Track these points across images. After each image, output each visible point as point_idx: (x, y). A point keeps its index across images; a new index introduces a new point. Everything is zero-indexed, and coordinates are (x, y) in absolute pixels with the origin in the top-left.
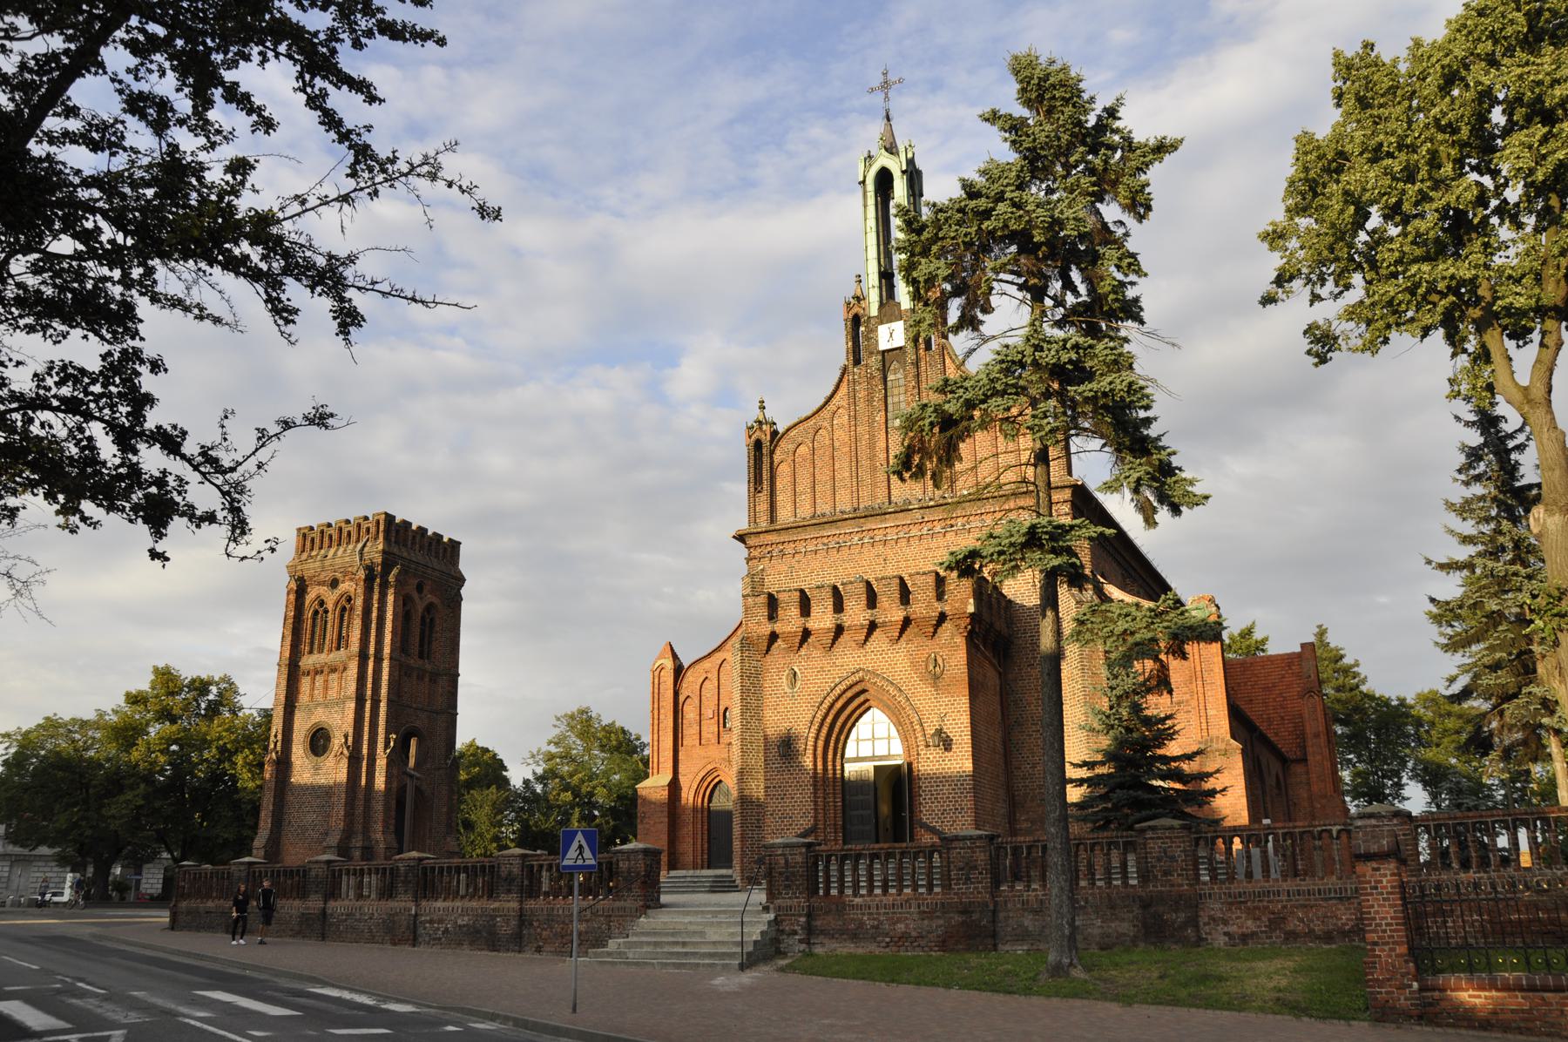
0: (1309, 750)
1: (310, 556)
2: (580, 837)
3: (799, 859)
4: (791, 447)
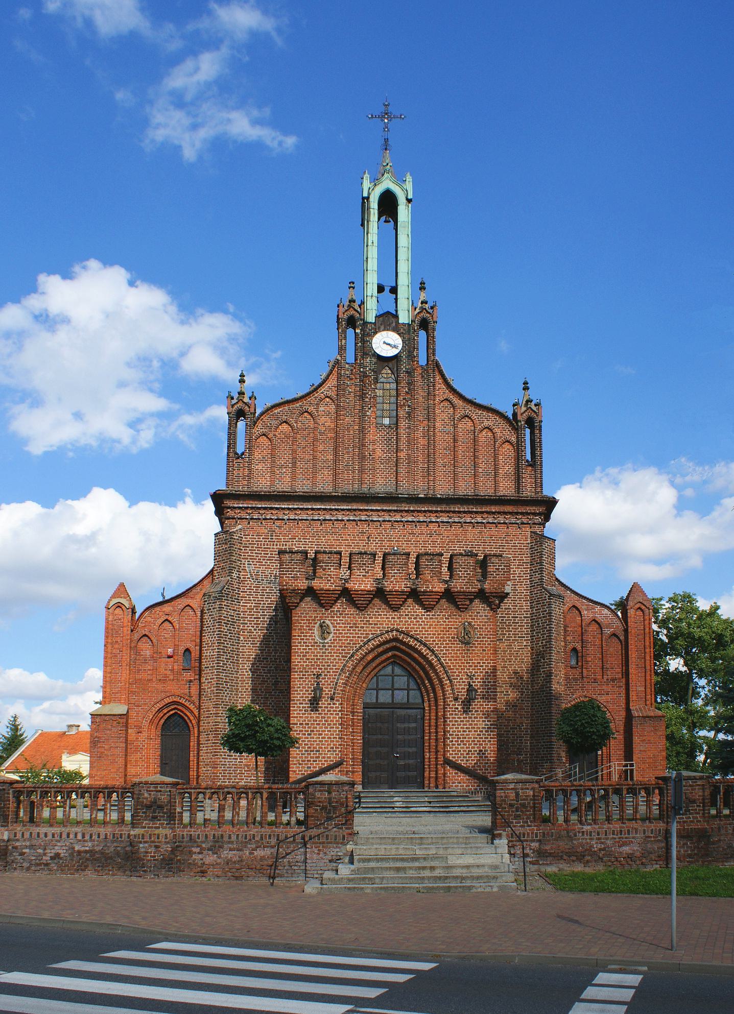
4: (274, 423)
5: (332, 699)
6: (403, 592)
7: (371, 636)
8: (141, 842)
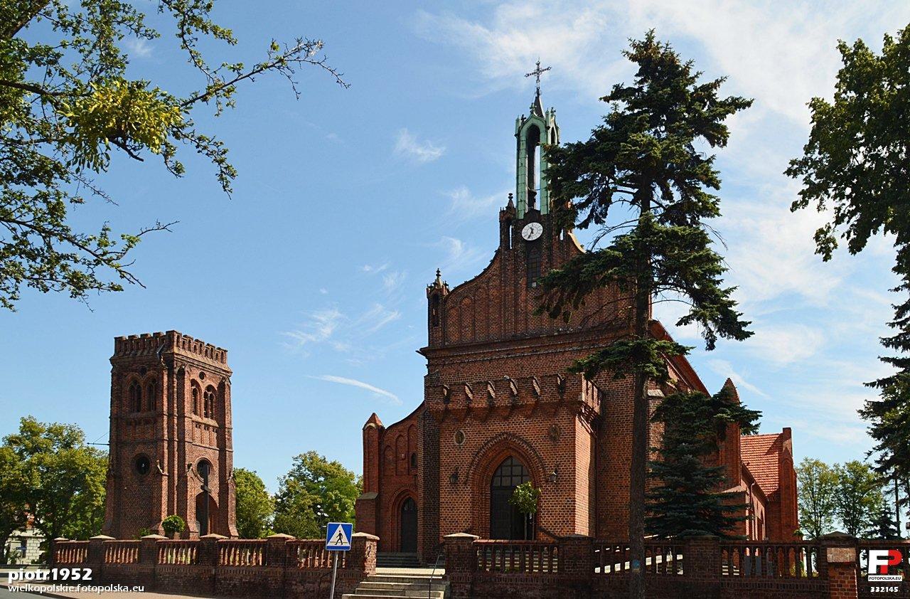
0: (782, 496)
1: (125, 354)
2: (340, 528)
5: (465, 483)
6: (507, 407)
7: (489, 439)
8: (269, 577)
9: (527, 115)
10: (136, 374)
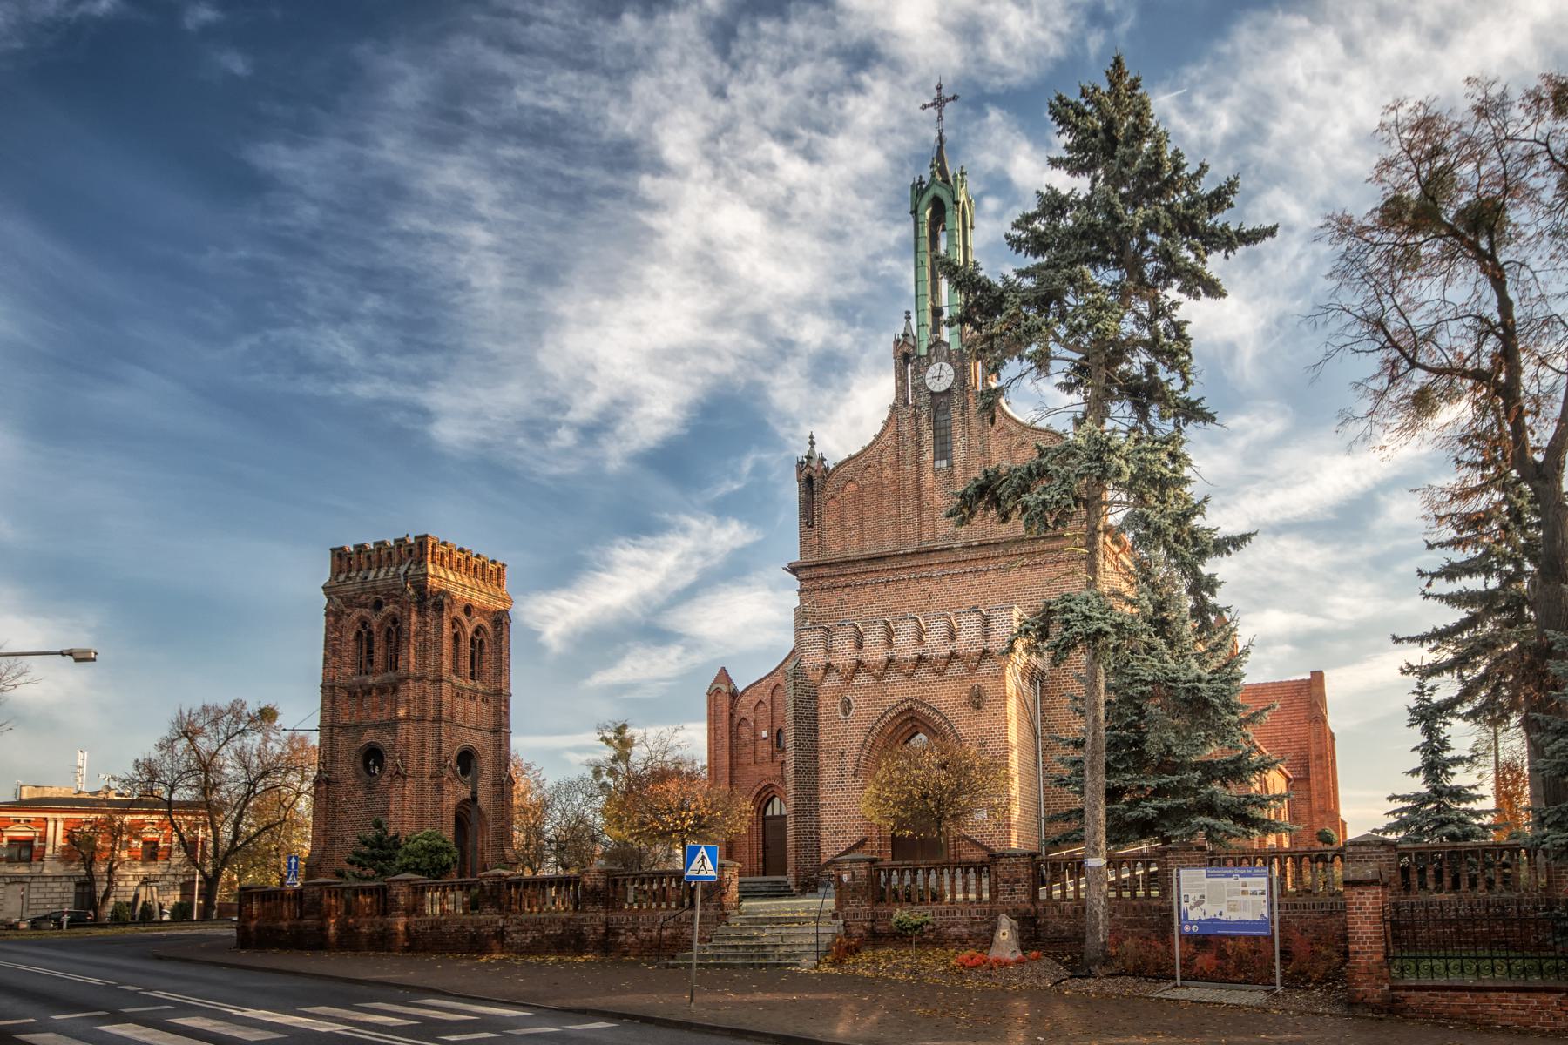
0: (1312, 770)
1: (348, 578)
3: (864, 872)
9: (927, 178)
10: (365, 612)
